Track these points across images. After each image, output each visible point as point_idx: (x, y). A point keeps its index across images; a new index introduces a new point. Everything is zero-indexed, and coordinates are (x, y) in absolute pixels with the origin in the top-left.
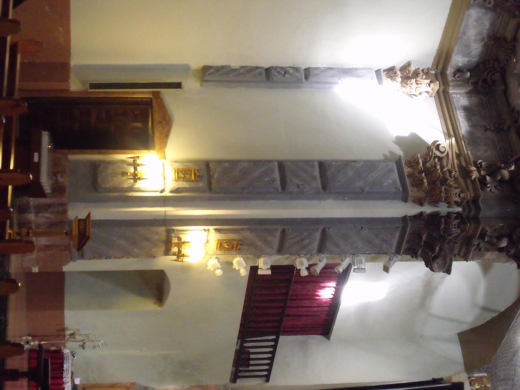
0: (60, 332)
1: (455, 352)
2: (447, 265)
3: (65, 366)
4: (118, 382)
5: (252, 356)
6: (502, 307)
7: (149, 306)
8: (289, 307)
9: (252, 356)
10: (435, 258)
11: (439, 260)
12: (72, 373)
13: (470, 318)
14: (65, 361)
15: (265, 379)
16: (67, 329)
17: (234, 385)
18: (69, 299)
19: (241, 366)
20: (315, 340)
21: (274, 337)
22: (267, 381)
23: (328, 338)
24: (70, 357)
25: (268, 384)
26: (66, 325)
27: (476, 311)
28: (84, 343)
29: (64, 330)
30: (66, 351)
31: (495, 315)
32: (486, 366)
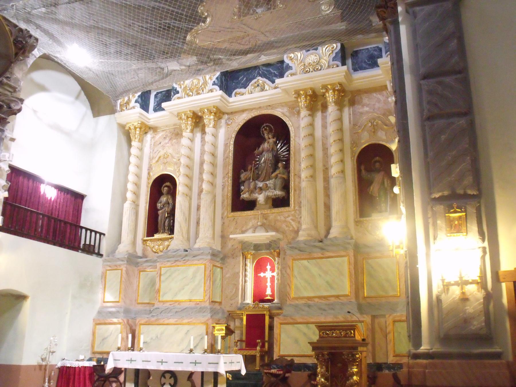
0: (41, 368)
1: (104, 119)
2: (16, 100)
3: (68, 366)
4: (91, 331)
5: (88, 243)
6: (79, 88)
7: (27, 305)
8: (58, 217)
9: (88, 243)
10: (10, 107)
11: (12, 105)
12: (77, 360)
13: (83, 108)
14: (65, 365)
15: (102, 236)
16: (409, 351)
17: (104, 256)
18: (15, 361)
19: (94, 250)
20: (86, 204)
21: (84, 230)
22: (104, 235)
23: (86, 196)
24: (64, 361)
25: (106, 235)
26: (36, 364)
27: (78, 103)
28: (50, 352)
29: (40, 366)
30: (59, 365)
31: (83, 93)
32: (113, 102)
